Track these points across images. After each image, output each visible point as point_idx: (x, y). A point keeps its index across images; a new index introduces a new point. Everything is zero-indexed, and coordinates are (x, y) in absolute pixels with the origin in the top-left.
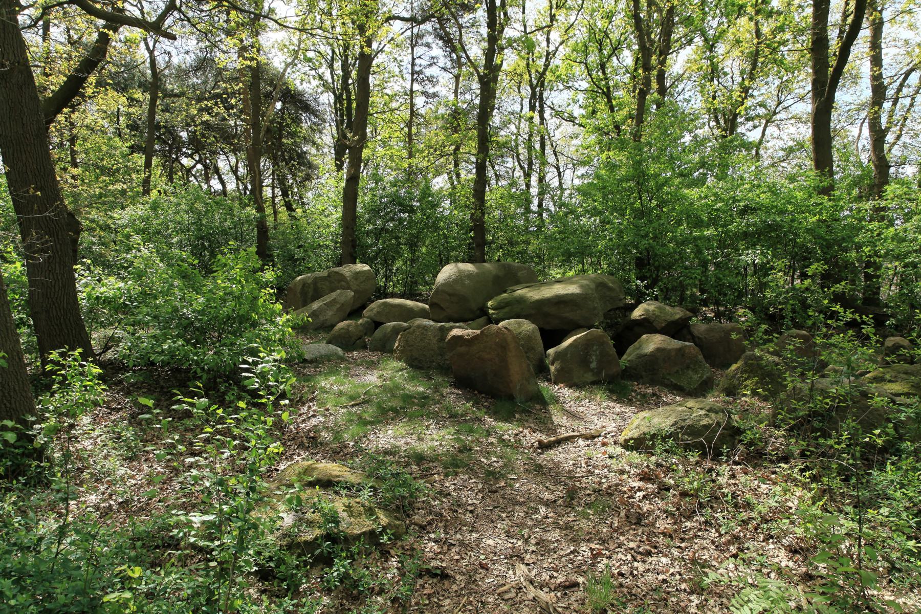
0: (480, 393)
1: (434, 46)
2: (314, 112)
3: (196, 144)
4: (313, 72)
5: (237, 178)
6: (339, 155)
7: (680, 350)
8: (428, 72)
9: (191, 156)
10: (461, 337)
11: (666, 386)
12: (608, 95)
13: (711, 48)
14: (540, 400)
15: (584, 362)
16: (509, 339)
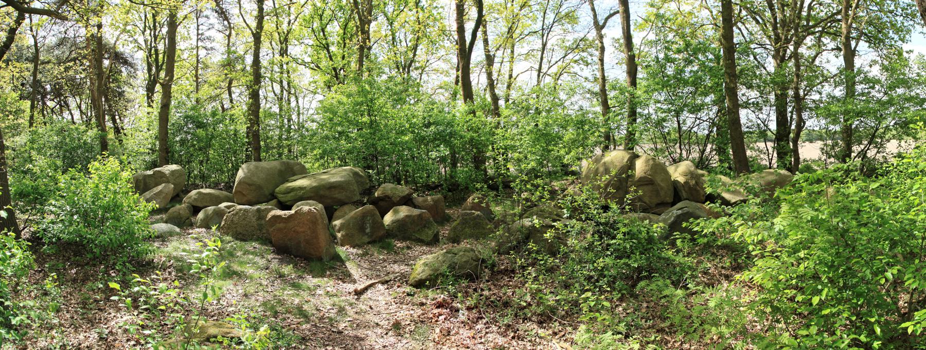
0: (296, 257)
1: (211, 17)
2: (131, 65)
3: (57, 93)
4: (131, 39)
5: (81, 111)
6: (150, 90)
7: (420, 216)
8: (207, 34)
9: (53, 100)
10: (279, 216)
11: (414, 240)
12: (327, 47)
13: (391, 24)
14: (337, 258)
15: (362, 229)
16: (318, 216)
